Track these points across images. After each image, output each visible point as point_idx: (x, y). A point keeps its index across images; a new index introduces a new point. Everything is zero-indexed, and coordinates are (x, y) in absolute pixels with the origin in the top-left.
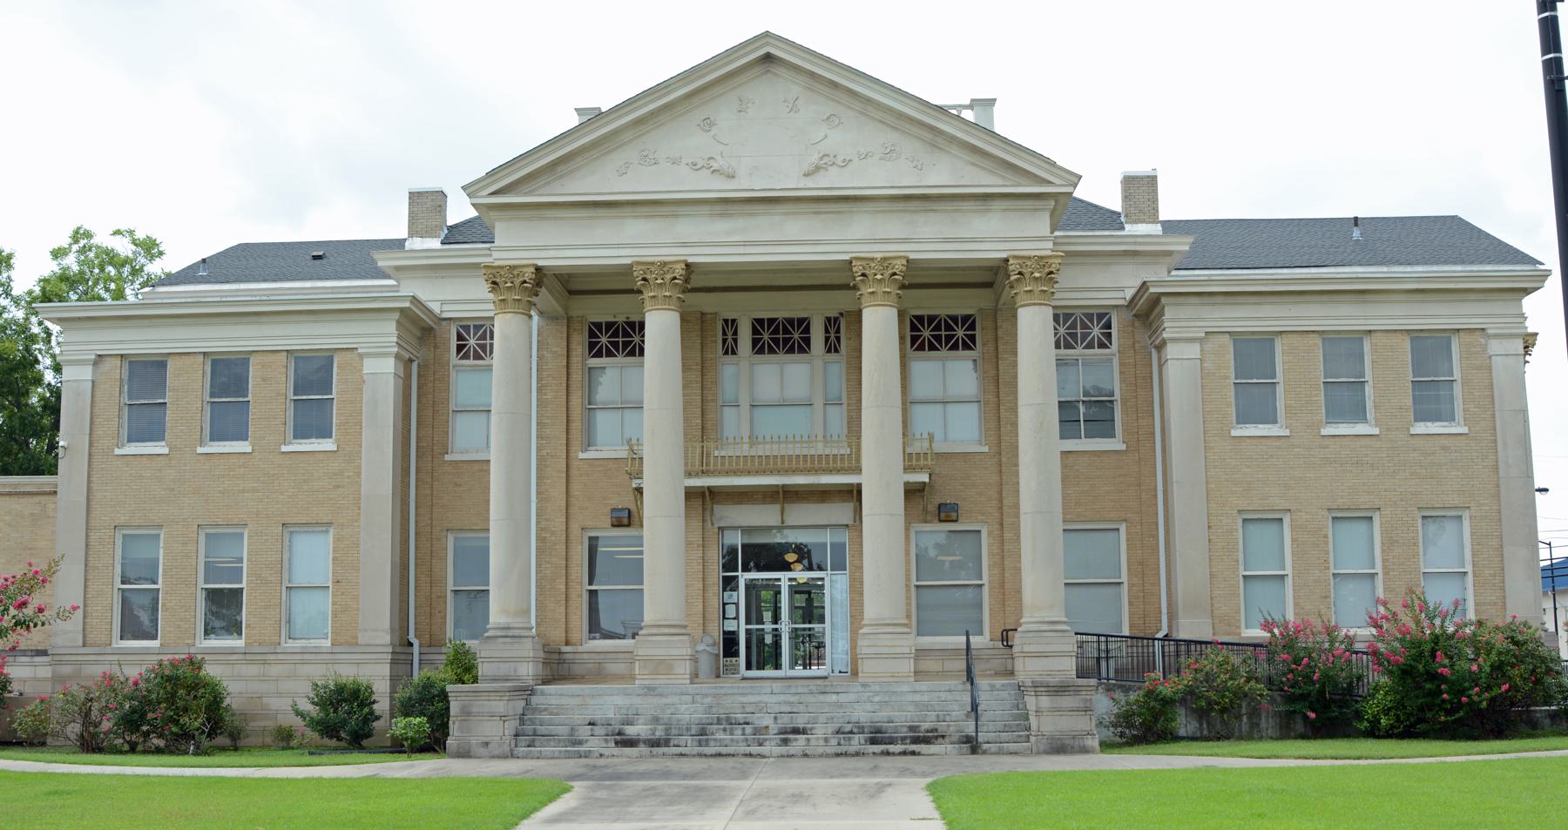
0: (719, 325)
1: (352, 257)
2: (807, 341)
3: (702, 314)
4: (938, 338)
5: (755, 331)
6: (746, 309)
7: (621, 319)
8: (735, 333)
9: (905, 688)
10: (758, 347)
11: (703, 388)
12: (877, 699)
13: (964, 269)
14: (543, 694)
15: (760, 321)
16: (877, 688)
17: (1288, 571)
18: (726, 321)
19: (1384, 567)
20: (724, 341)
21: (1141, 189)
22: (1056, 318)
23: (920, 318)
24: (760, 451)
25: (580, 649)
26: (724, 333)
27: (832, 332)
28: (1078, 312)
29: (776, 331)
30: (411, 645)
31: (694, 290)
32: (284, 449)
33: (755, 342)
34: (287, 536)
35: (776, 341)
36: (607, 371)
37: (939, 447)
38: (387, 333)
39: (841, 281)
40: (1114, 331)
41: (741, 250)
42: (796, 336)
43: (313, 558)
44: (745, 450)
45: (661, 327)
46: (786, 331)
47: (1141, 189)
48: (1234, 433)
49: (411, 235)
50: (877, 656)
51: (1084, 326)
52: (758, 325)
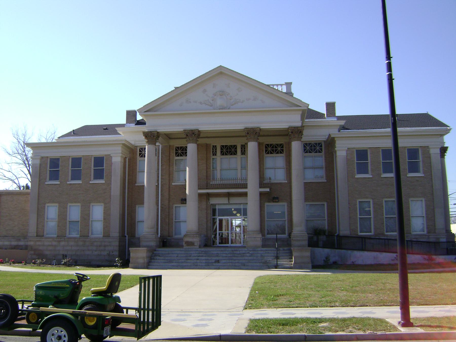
0: (212, 147)
2: (236, 151)
3: (207, 144)
4: (273, 150)
5: (221, 149)
6: (219, 143)
8: (216, 149)
10: (222, 153)
11: (207, 165)
14: (158, 251)
15: (223, 146)
16: (251, 249)
18: (213, 146)
20: (213, 152)
21: (331, 107)
23: (268, 145)
24: (225, 182)
26: (213, 150)
28: (313, 142)
29: (227, 149)
30: (126, 237)
32: (91, 182)
33: (221, 152)
35: (227, 152)
38: (119, 149)
43: (97, 212)
45: (252, 147)
46: (230, 149)
47: (331, 107)
48: (356, 177)
49: (127, 123)
52: (222, 147)
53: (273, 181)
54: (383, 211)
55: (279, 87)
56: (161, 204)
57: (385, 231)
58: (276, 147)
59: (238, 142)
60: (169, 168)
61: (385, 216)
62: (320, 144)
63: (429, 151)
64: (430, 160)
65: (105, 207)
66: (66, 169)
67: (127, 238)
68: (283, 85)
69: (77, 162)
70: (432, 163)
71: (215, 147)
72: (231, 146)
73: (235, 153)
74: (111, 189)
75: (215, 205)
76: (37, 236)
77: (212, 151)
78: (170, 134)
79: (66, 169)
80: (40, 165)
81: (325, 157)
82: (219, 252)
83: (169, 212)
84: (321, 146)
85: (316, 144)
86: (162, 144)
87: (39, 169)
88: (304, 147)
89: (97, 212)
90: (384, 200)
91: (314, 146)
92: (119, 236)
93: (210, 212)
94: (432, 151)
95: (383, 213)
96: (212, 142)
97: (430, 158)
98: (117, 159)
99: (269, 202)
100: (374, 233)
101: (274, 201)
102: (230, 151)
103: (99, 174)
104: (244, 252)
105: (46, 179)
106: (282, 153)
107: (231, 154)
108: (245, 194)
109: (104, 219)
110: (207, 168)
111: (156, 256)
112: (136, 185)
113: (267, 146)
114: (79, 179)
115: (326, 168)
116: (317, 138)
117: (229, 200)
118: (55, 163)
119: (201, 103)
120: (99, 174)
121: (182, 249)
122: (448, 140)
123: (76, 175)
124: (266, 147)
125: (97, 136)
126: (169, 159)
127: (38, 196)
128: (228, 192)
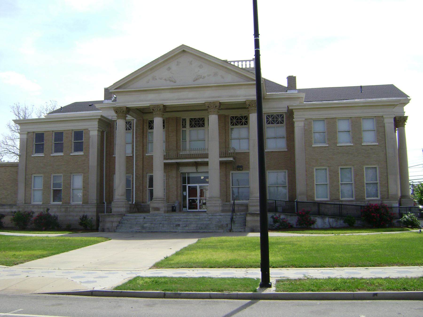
0: (181, 120)
1: (90, 105)
2: (204, 124)
3: (177, 118)
4: (238, 122)
5: (190, 122)
6: (188, 116)
7: (239, 116)
8: (185, 122)
9: (218, 214)
10: (191, 126)
11: (177, 137)
12: (210, 217)
13: (188, 106)
14: (127, 216)
15: (192, 119)
16: (210, 214)
17: (378, 182)
18: (183, 119)
19: (380, 181)
20: (183, 124)
21: (292, 80)
22: (126, 123)
23: (233, 117)
24: (192, 152)
25: (146, 204)
26: (183, 122)
27: (184, 122)
28: (275, 114)
29: (196, 121)
30: (104, 203)
31: (222, 109)
32: (71, 154)
33: (190, 124)
34: (72, 175)
35: (196, 124)
36: (234, 129)
37: (237, 151)
38: (96, 124)
39: (205, 108)
40: (284, 119)
41: (178, 101)
42: (193, 123)
43: (78, 181)
44: (188, 152)
45: (213, 120)
46: (198, 121)
47: (292, 80)
48: (313, 146)
49: (105, 99)
50: (255, 206)
51: (276, 118)
52: (191, 120)
53: (238, 151)
54: (338, 177)
55: (240, 63)
56: (136, 174)
57: (366, 195)
58: (240, 119)
60: (143, 141)
61: (340, 182)
62: (281, 116)
63: (383, 121)
64: (384, 129)
65: (84, 177)
66: (49, 142)
67: (105, 204)
68: (252, 60)
69: (59, 136)
70: (386, 132)
72: (199, 119)
74: (89, 160)
75: (185, 173)
76: (25, 203)
77: (181, 123)
78: (143, 108)
79: (49, 142)
80: (27, 139)
81: (286, 128)
82: (181, 217)
83: (143, 181)
84: (283, 118)
85: (278, 115)
86: (136, 118)
87: (26, 143)
89: (78, 181)
90: (340, 167)
91: (276, 118)
92: (97, 203)
93: (180, 180)
94: (386, 121)
96: (183, 115)
97: (384, 127)
98: (94, 134)
99: (234, 170)
100: (330, 198)
101: (238, 169)
102: (198, 124)
104: (203, 217)
106: (246, 125)
107: (200, 127)
108: (206, 164)
109: (84, 187)
110: (177, 140)
114: (62, 151)
115: (287, 138)
116: (279, 109)
117: (197, 169)
118: (40, 137)
119: (165, 80)
120: (79, 147)
121: (148, 214)
122: (407, 110)
123: (59, 148)
124: (231, 120)
125: (69, 113)
126: (143, 132)
127: (26, 168)
128: (195, 162)
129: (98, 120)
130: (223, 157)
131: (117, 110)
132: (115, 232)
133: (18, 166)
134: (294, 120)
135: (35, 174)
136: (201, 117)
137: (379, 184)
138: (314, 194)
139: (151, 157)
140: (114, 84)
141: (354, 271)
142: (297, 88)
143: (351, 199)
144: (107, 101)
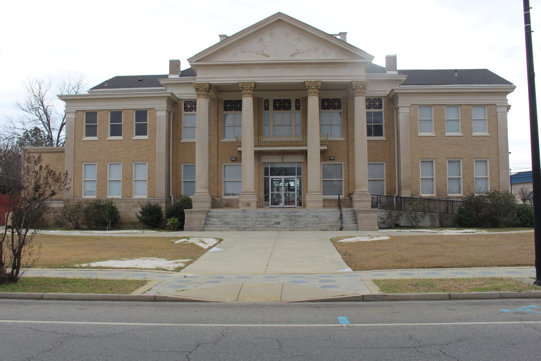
2: (290, 106)
3: (259, 98)
5: (274, 103)
8: (268, 104)
10: (275, 108)
17: (434, 177)
20: (265, 106)
26: (265, 104)
31: (257, 91)
32: (133, 138)
33: (274, 107)
40: (183, 107)
43: (141, 172)
44: (271, 139)
45: (248, 103)
49: (170, 73)
50: (312, 201)
52: (275, 101)
59: (293, 97)
62: (379, 100)
64: (497, 119)
67: (172, 199)
71: (267, 101)
73: (289, 108)
77: (264, 105)
79: (104, 124)
85: (375, 99)
88: (322, 102)
89: (141, 172)
93: (262, 171)
95: (446, 174)
97: (497, 116)
103: (141, 130)
105: (82, 135)
109: (149, 178)
111: (210, 217)
112: (181, 141)
113: (226, 102)
118: (91, 116)
120: (141, 130)
123: (116, 131)
129: (166, 99)
130: (258, 146)
131: (198, 88)
132: (204, 231)
133: (64, 152)
134: (399, 105)
135: (85, 162)
136: (287, 98)
137: (462, 180)
138: (419, 189)
139: (193, 145)
140: (195, 56)
141: (485, 271)
142: (398, 69)
143: (459, 195)
144: (172, 76)
